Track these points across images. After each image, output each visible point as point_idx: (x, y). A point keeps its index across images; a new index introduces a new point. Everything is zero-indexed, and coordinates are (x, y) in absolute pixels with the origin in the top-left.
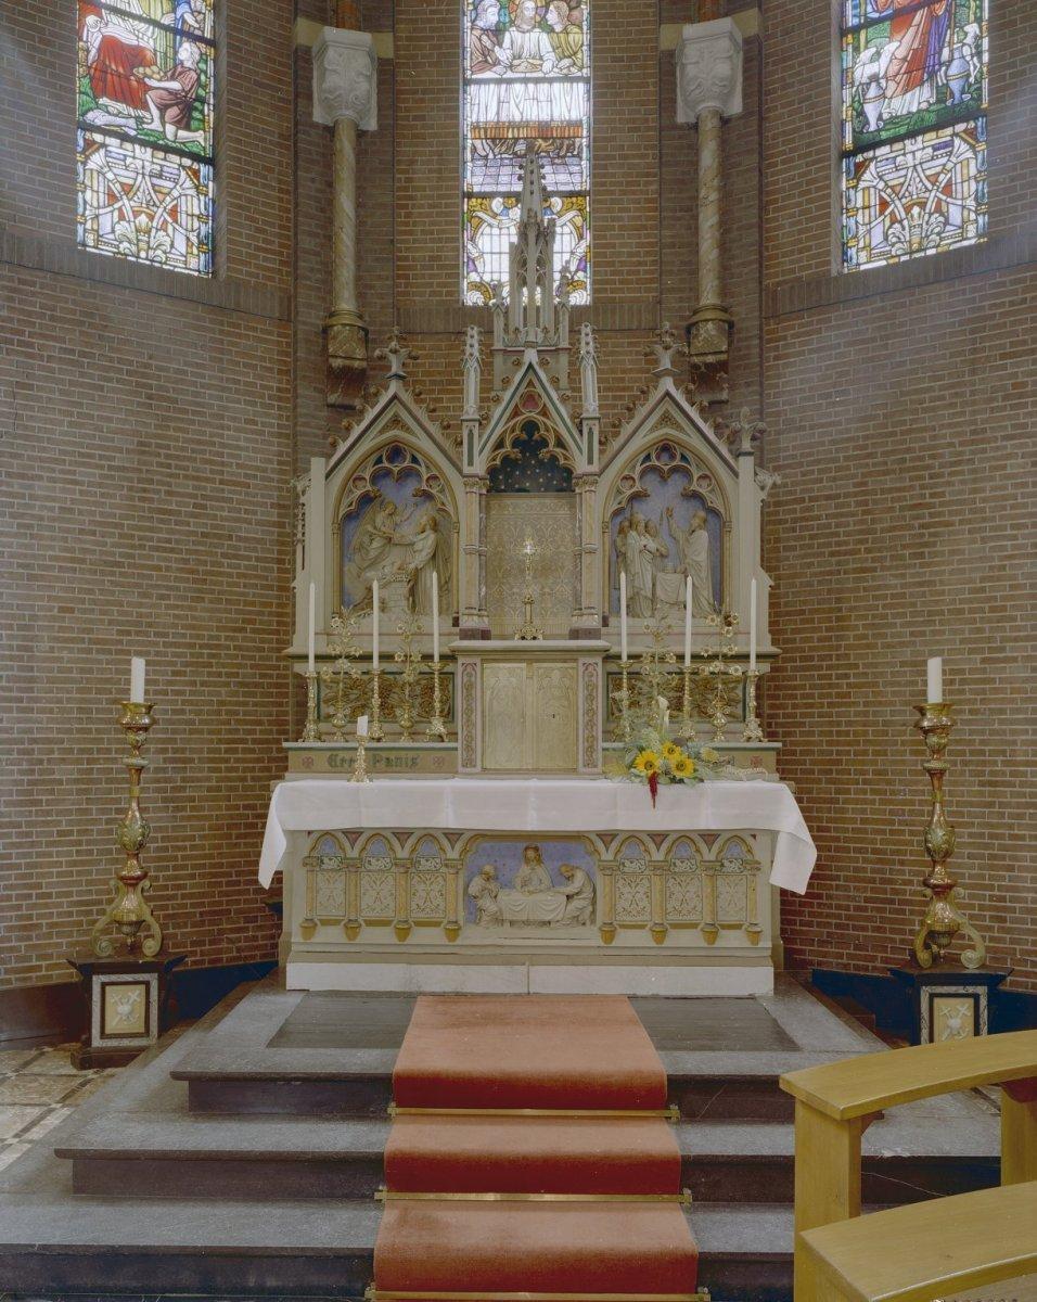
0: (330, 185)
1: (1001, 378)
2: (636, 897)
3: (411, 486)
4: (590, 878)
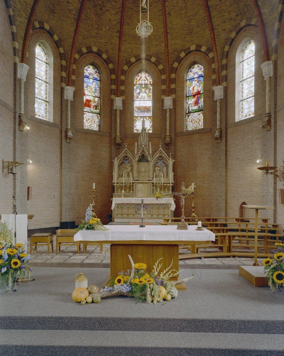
0: (116, 117)
1: (204, 147)
2: (155, 211)
3: (128, 161)
4: (150, 209)
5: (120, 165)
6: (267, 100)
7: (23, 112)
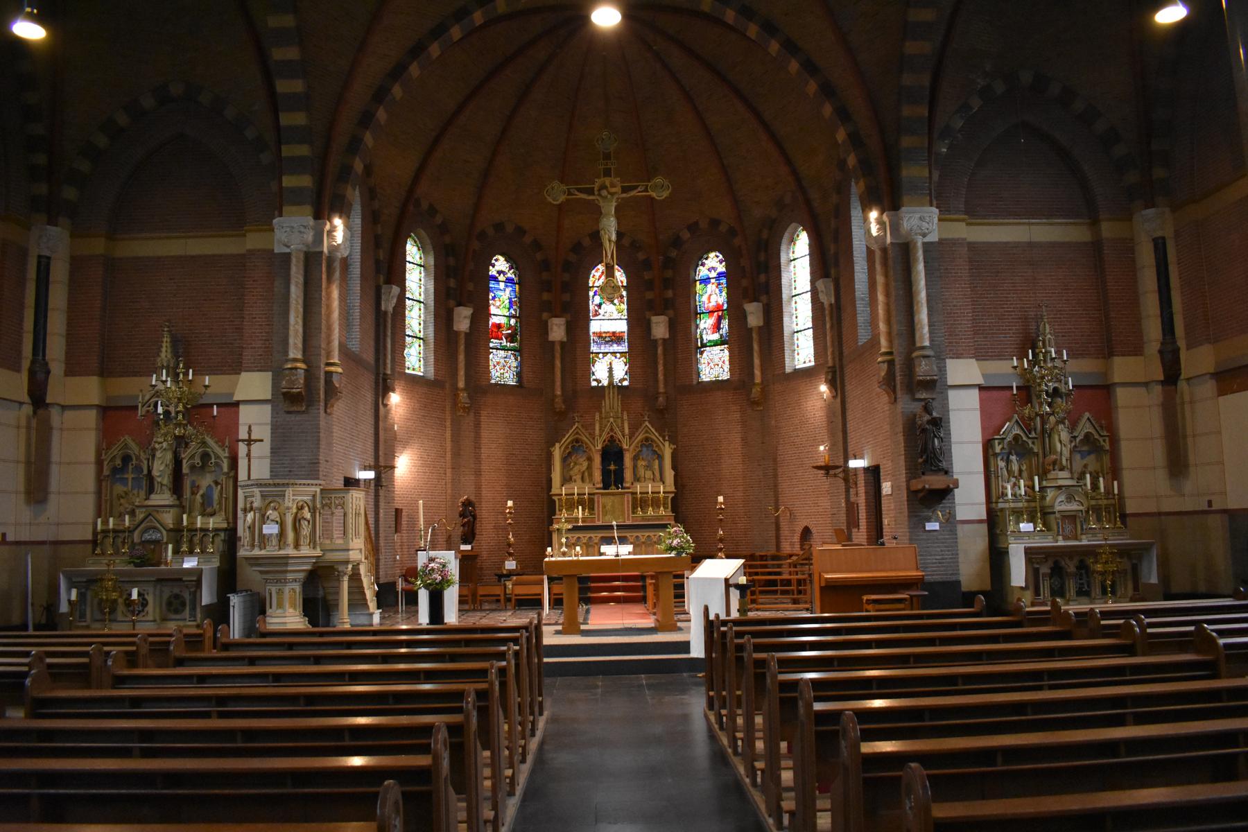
5: (565, 460)
6: (829, 344)
7: (389, 372)
